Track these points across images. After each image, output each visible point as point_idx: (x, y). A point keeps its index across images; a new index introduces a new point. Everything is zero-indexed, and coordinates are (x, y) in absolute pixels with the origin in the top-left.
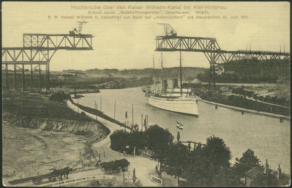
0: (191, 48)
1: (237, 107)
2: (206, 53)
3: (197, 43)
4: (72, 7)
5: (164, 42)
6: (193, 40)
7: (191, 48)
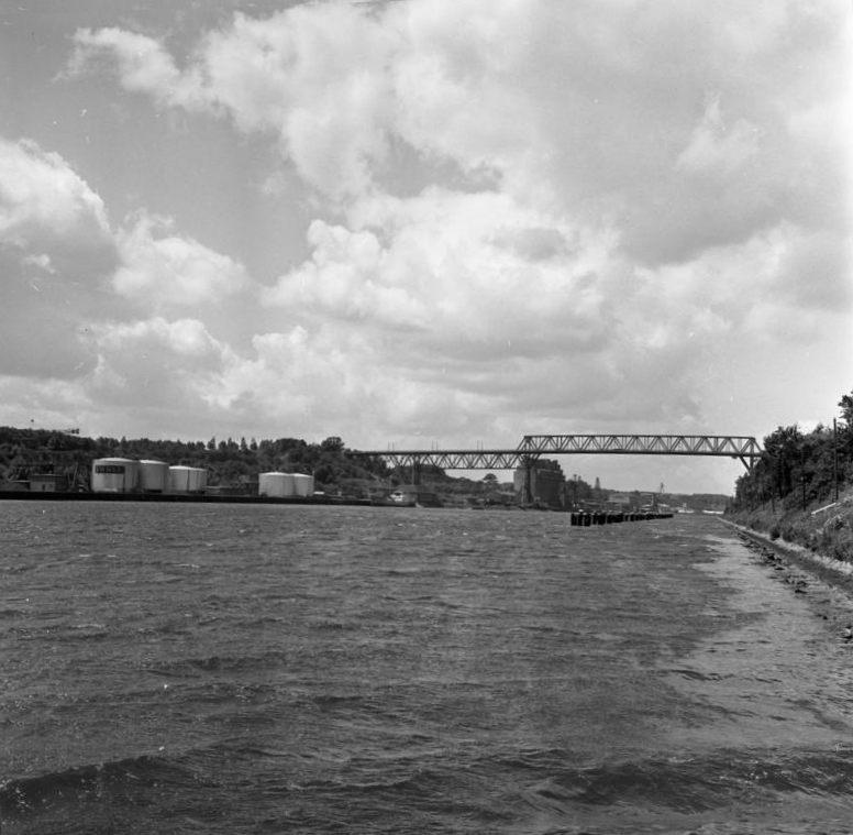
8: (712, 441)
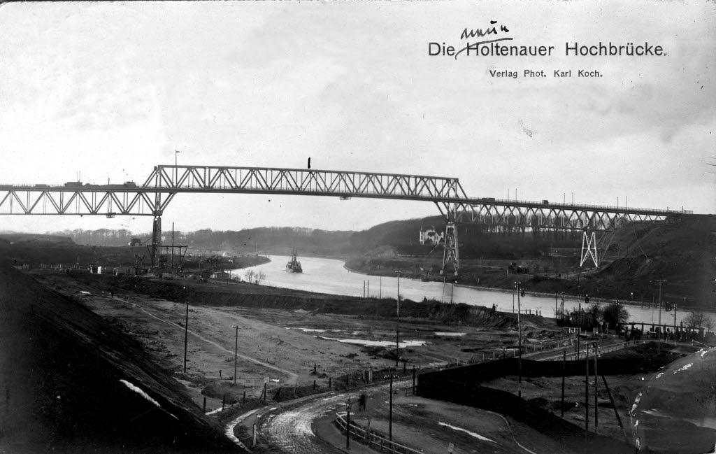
0: (271, 186)
1: (504, 285)
2: (440, 204)
3: (253, 176)
4: (567, 49)
5: (187, 178)
6: (214, 172)
7: (271, 186)
8: (439, 184)
